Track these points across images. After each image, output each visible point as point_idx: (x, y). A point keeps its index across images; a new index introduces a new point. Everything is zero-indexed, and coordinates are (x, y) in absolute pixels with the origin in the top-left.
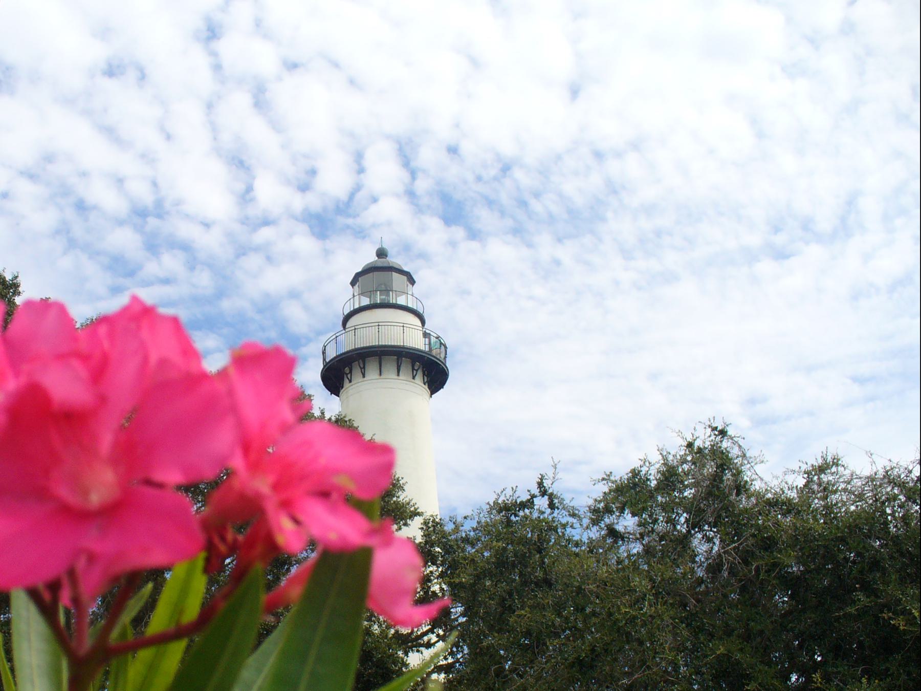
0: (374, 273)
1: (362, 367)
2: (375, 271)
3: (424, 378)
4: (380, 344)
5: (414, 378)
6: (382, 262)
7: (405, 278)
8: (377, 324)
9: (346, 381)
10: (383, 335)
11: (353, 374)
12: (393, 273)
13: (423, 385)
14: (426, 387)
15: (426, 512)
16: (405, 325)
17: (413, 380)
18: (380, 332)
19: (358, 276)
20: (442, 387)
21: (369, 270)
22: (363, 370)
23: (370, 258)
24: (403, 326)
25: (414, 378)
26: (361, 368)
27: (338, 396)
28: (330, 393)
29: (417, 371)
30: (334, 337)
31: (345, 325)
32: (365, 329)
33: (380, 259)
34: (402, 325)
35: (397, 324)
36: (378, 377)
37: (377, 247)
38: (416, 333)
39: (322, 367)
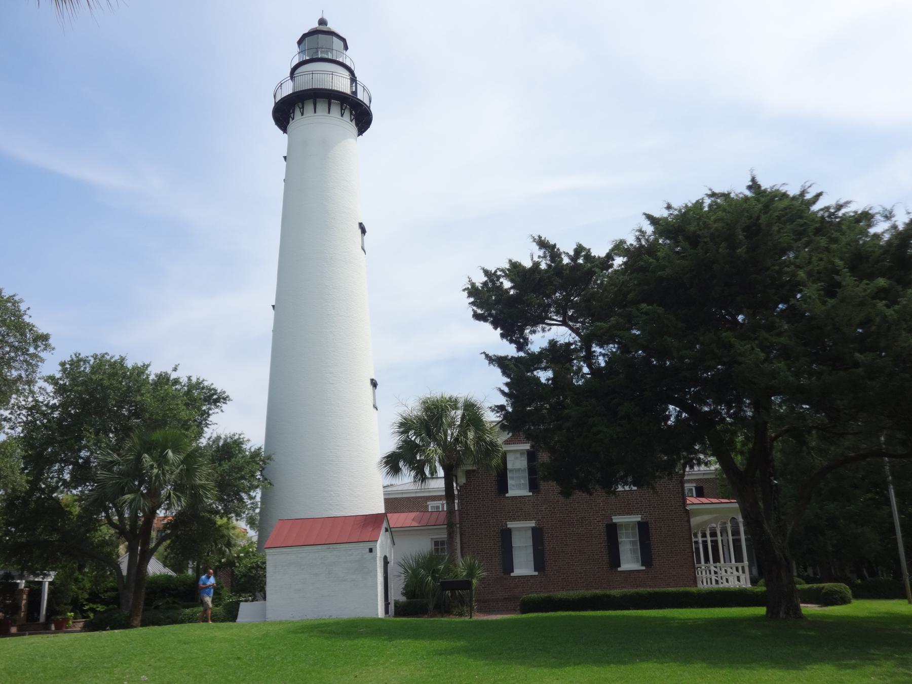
0: (319, 35)
1: (301, 107)
2: (320, 34)
3: (351, 116)
4: (314, 87)
5: (342, 115)
6: (323, 28)
7: (342, 43)
8: (311, 72)
9: (291, 119)
10: (316, 82)
11: (295, 114)
12: (334, 37)
13: (350, 122)
14: (354, 123)
15: (531, 343)
17: (329, 115)
18: (314, 79)
19: (305, 36)
20: (369, 127)
21: (313, 33)
22: (302, 110)
23: (315, 25)
24: (332, 74)
25: (342, 115)
26: (300, 108)
27: (286, 133)
28: (283, 132)
29: (344, 110)
31: (295, 71)
33: (320, 26)
34: (331, 73)
35: (300, 74)
36: (313, 114)
37: (320, 17)
38: (340, 80)
39: (274, 105)
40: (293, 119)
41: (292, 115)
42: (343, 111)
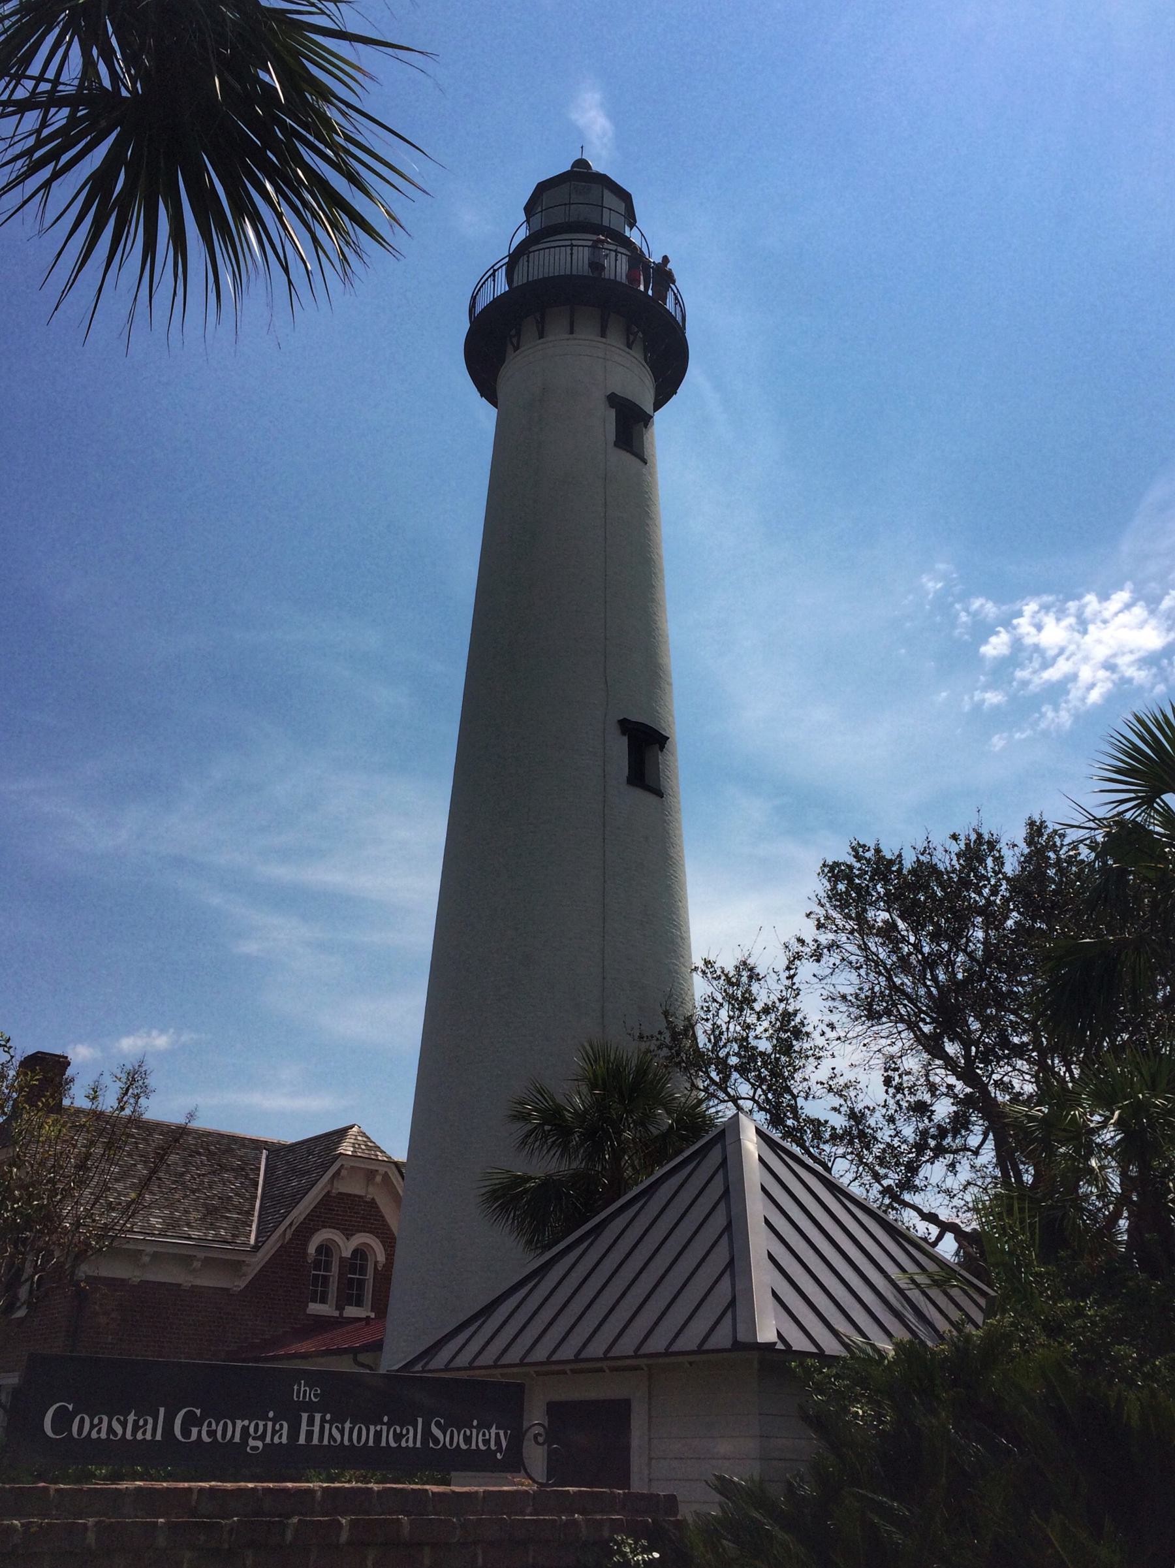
4: (574, 273)
5: (629, 346)
8: (568, 243)
9: (510, 349)
14: (637, 354)
16: (574, 242)
30: (491, 271)
32: (547, 251)
40: (516, 348)
41: (515, 340)
42: (632, 337)
